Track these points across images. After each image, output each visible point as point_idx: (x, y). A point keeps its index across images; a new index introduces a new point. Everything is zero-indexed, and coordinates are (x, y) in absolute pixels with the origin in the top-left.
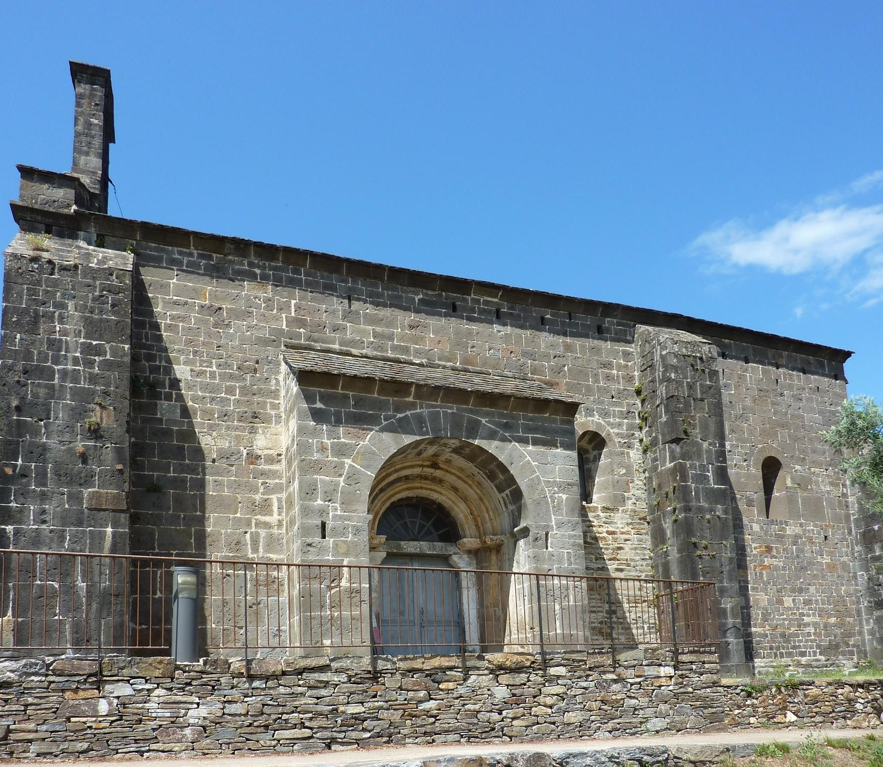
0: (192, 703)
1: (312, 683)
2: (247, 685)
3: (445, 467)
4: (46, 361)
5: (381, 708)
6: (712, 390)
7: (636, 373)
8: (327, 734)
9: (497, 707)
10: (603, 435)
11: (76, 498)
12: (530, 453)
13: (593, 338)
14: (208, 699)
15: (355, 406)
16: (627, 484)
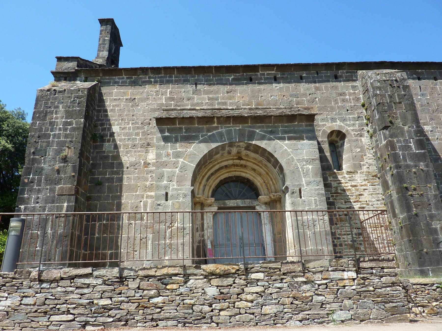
0: (3, 297)
1: (79, 285)
2: (38, 286)
3: (246, 158)
4: (48, 131)
5: (122, 302)
6: (406, 97)
7: (361, 96)
8: (83, 318)
9: (208, 302)
10: (344, 131)
11: (52, 190)
12: (286, 145)
13: (333, 82)
14: (14, 294)
15: (185, 132)
16: (362, 157)
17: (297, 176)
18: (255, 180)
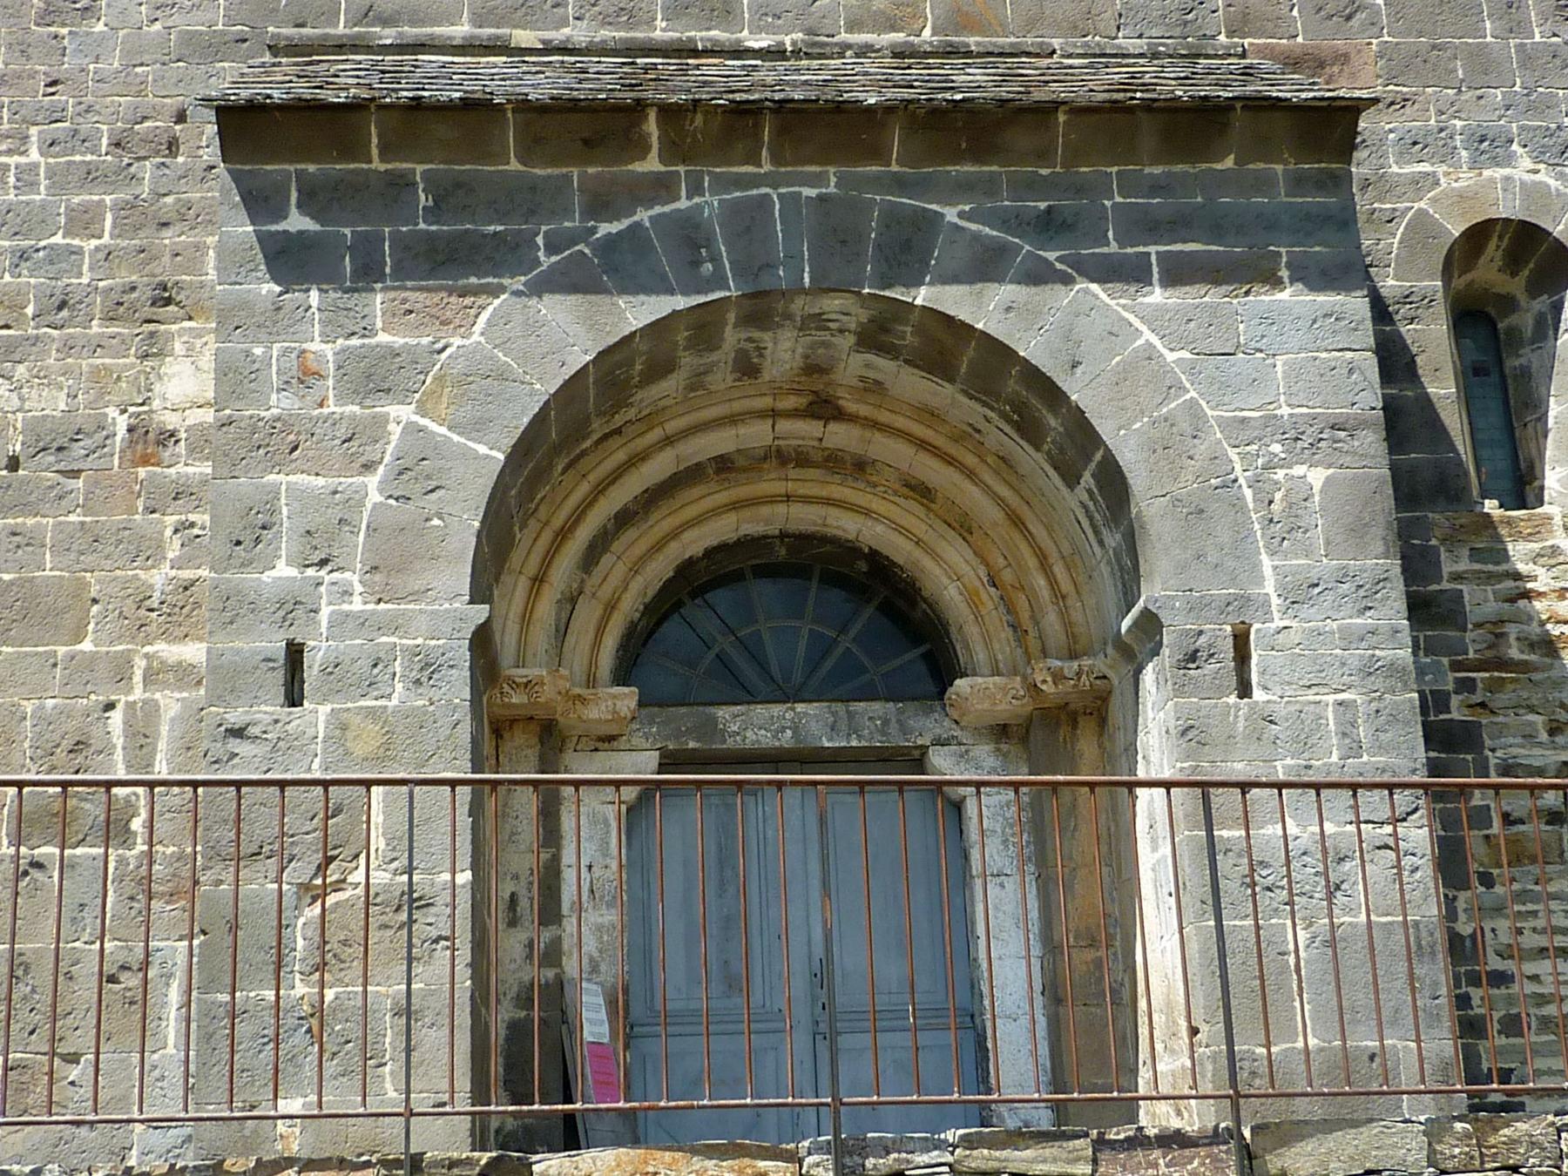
3: (864, 410)
12: (1153, 319)
15: (433, 214)
17: (1225, 537)
18: (928, 563)
